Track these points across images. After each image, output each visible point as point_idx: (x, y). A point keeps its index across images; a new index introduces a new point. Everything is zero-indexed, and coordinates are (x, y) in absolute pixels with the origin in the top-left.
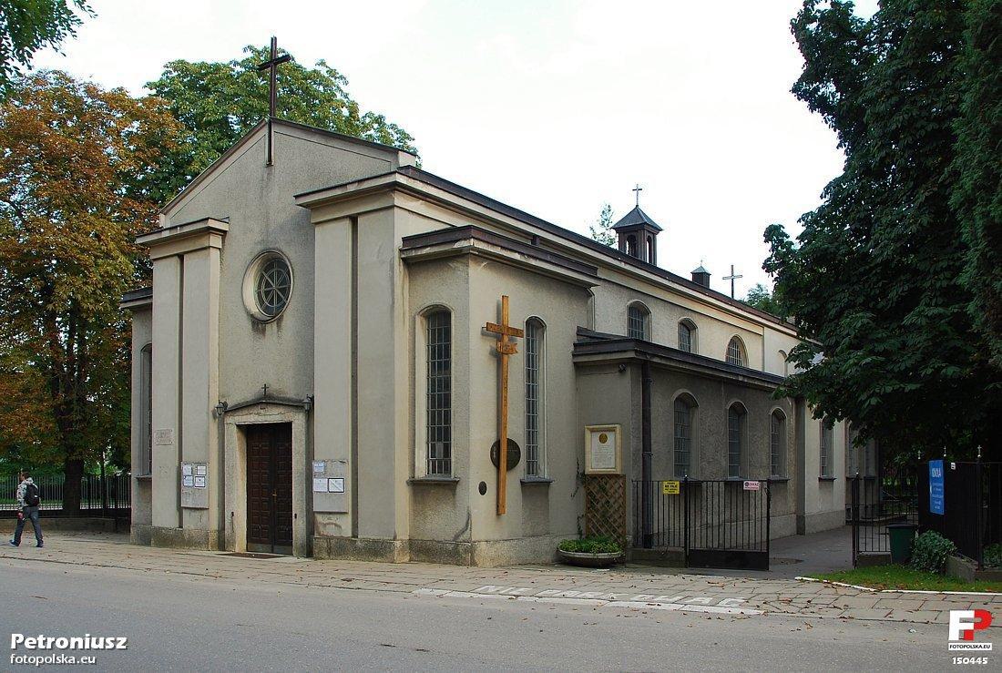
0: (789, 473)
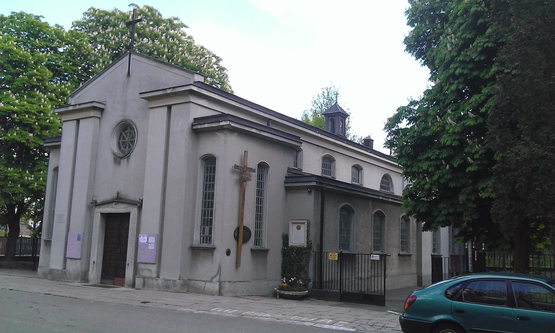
0: (413, 250)
